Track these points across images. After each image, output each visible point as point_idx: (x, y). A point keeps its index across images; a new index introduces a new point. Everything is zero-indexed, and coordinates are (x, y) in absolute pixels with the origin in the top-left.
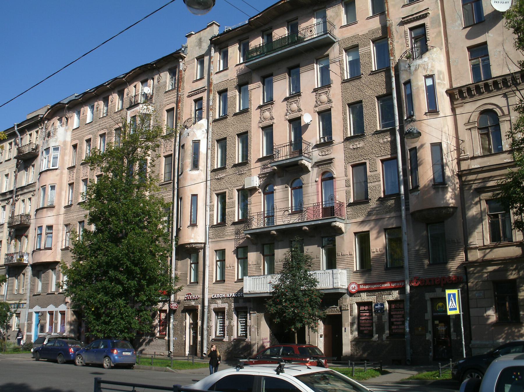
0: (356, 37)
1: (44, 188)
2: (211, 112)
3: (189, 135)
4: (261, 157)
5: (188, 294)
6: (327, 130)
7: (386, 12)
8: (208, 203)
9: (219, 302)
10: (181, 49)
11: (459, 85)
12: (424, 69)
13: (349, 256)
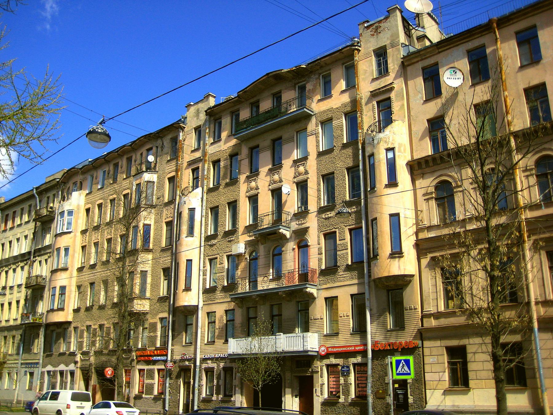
0: (330, 110)
1: (58, 249)
2: (205, 182)
3: (185, 203)
4: (248, 224)
5: (183, 354)
6: (304, 200)
7: (357, 86)
8: (202, 268)
9: (209, 362)
10: (180, 120)
11: (419, 157)
12: (386, 142)
13: (320, 320)
